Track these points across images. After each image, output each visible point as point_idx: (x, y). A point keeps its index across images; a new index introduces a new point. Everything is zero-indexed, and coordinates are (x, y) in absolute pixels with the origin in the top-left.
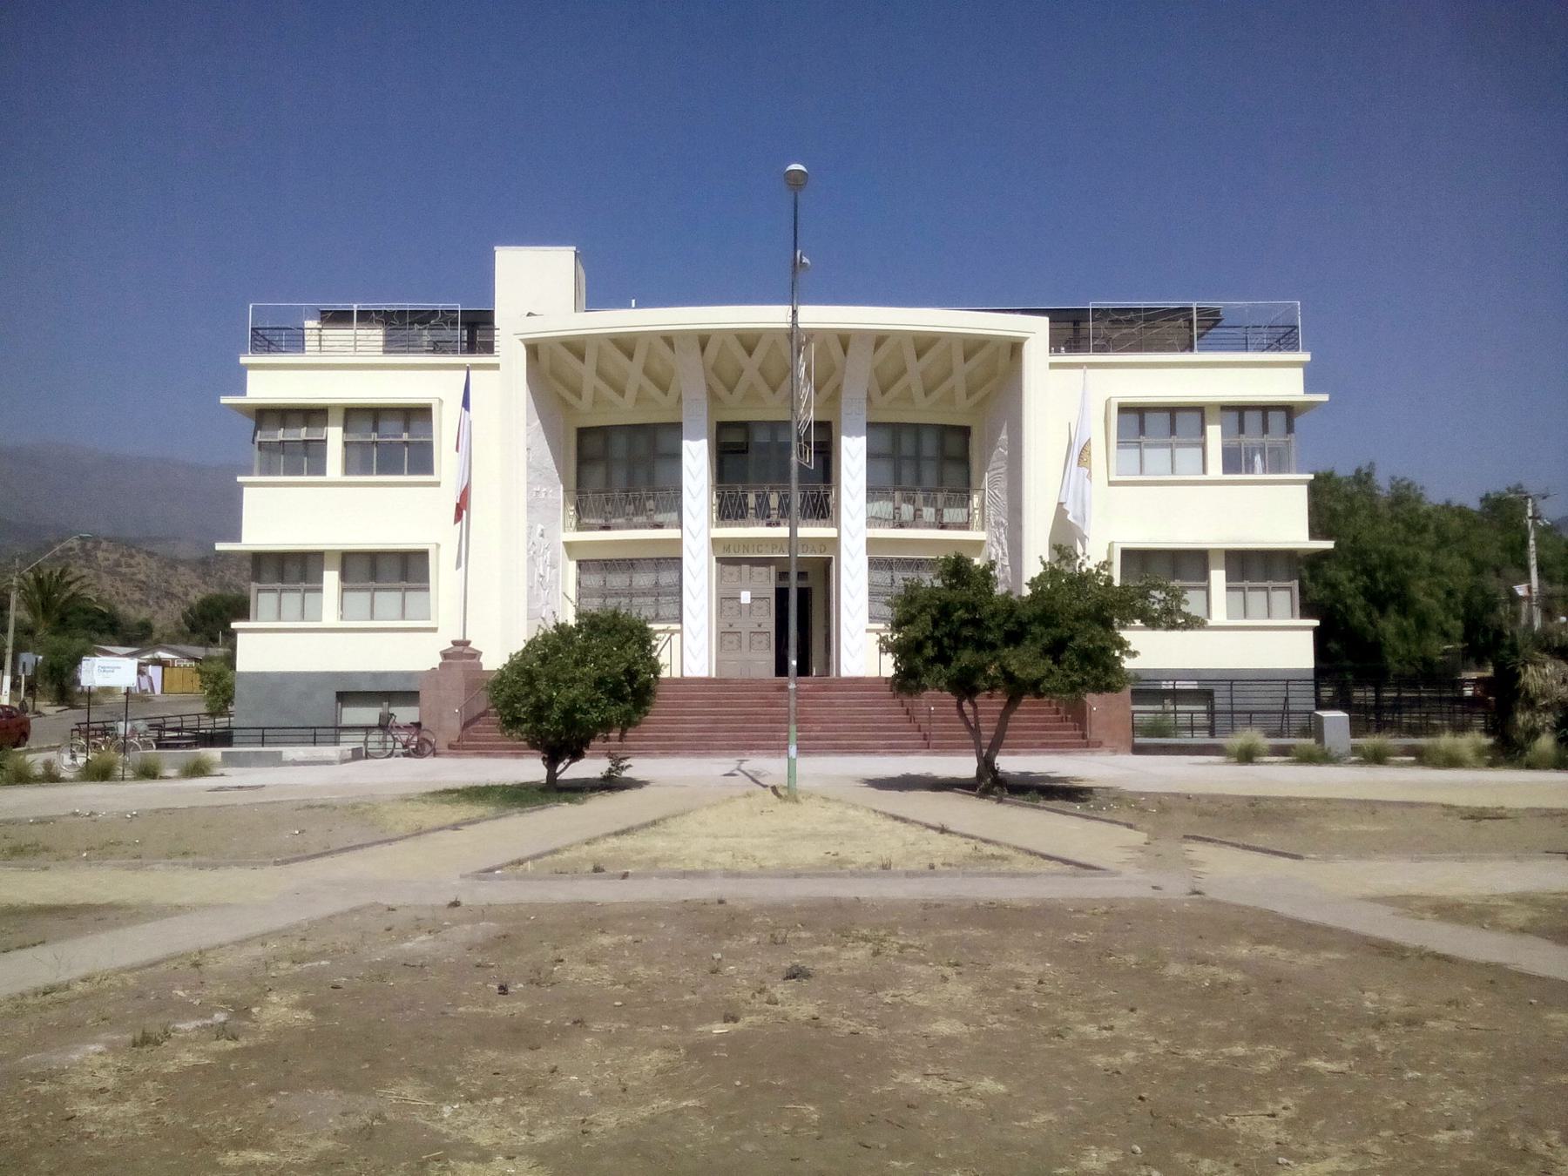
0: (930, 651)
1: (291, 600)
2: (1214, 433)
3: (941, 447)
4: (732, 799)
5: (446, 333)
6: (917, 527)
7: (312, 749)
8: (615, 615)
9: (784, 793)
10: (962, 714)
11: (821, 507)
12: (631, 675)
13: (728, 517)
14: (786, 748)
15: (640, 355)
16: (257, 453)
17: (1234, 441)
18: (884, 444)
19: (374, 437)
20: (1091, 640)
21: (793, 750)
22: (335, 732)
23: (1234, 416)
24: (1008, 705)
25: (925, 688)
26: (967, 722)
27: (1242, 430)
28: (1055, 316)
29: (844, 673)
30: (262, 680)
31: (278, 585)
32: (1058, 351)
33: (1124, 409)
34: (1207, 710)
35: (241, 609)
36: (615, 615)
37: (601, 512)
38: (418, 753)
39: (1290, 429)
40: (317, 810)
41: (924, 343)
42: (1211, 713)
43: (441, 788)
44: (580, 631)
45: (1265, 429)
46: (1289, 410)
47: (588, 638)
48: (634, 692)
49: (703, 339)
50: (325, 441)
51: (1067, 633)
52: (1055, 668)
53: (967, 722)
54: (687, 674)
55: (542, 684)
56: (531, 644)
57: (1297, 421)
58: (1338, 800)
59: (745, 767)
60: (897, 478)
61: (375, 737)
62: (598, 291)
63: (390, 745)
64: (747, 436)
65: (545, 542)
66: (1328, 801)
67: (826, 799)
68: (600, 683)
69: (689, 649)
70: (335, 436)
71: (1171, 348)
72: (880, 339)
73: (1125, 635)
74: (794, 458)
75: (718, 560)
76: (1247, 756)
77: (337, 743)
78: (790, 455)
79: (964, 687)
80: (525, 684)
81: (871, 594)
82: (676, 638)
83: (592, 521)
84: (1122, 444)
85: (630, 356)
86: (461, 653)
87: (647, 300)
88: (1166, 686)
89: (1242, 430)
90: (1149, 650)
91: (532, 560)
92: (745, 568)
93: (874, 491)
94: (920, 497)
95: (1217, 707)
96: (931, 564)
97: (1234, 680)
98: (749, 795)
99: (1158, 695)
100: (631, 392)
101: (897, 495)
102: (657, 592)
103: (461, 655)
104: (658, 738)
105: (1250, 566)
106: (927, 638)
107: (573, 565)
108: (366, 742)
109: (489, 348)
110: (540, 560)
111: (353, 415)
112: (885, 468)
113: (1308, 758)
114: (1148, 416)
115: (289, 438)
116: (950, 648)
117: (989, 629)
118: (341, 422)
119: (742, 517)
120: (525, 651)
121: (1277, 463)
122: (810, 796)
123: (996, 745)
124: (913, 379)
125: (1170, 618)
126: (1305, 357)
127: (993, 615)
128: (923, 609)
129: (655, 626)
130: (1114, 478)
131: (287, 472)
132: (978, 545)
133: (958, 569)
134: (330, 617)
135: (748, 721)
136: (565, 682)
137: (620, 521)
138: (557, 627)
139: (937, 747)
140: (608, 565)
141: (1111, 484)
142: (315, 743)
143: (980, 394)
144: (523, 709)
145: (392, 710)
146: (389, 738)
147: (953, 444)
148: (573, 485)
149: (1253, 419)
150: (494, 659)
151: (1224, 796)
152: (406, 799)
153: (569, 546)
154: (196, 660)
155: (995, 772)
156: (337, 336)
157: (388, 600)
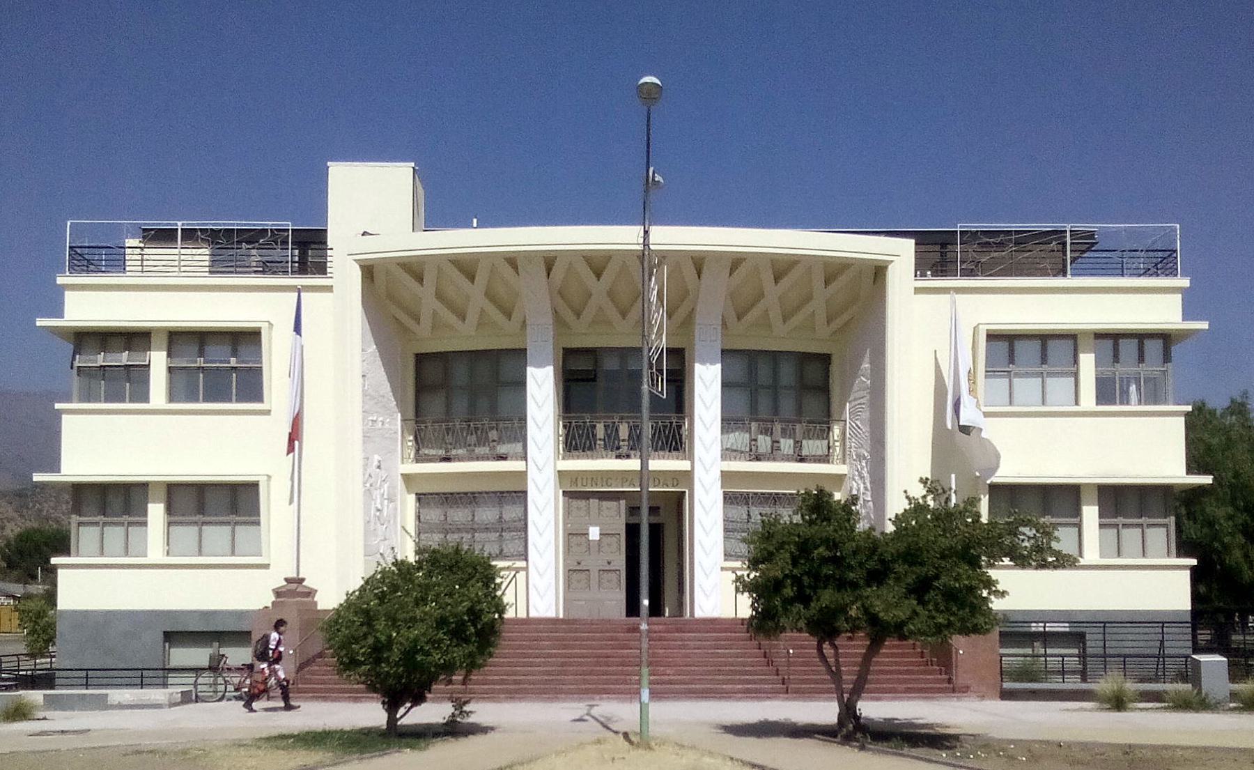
0: (788, 592)
1: (114, 534)
2: (1087, 361)
3: (801, 376)
4: (581, 745)
5: (276, 254)
6: (774, 460)
8: (457, 551)
9: (637, 739)
11: (674, 439)
12: (475, 614)
15: (607, 276)
17: (1108, 371)
18: (739, 373)
19: (200, 362)
22: (161, 674)
25: (783, 629)
27: (1116, 358)
28: (922, 239)
29: (699, 614)
31: (100, 518)
32: (923, 275)
33: (992, 337)
34: (1080, 651)
35: (62, 545)
37: (441, 443)
39: (1167, 358)
41: (782, 266)
42: (1083, 656)
43: (275, 733)
44: (420, 568)
45: (1141, 359)
46: (1166, 338)
47: (429, 575)
49: (549, 261)
50: (149, 365)
52: (919, 609)
54: (533, 614)
55: (381, 625)
59: (595, 711)
61: (206, 679)
62: (437, 210)
65: (383, 474)
66: (1205, 749)
67: (682, 746)
68: (442, 622)
69: (535, 588)
70: (158, 361)
71: (1044, 273)
72: (736, 261)
74: (645, 387)
76: (1118, 703)
77: (165, 685)
80: (362, 624)
81: (726, 530)
83: (432, 452)
84: (990, 373)
85: (471, 278)
86: (295, 590)
88: (1036, 628)
89: (1116, 358)
90: (1018, 590)
91: (368, 493)
92: (594, 502)
93: (729, 423)
94: (778, 427)
95: (1089, 651)
96: (790, 499)
97: (1106, 622)
98: (599, 742)
99: (1029, 638)
100: (472, 317)
101: (754, 425)
102: (501, 527)
103: (292, 593)
104: (502, 682)
105: (1123, 501)
106: (786, 576)
107: (411, 499)
110: (376, 494)
111: (177, 338)
112: (741, 399)
113: (1183, 704)
115: (109, 364)
116: (810, 587)
117: (851, 568)
118: (165, 345)
119: (590, 448)
121: (1154, 393)
122: (663, 742)
123: (859, 690)
125: (1041, 557)
126: (1185, 283)
128: (781, 546)
129: (499, 564)
132: (840, 479)
133: (818, 504)
134: (156, 553)
135: (598, 664)
136: (405, 621)
137: (460, 452)
138: (395, 564)
139: (797, 691)
140: (449, 499)
144: (361, 650)
150: (329, 598)
152: (240, 744)
153: (407, 478)
154: (14, 597)
156: (159, 254)
157: (217, 535)
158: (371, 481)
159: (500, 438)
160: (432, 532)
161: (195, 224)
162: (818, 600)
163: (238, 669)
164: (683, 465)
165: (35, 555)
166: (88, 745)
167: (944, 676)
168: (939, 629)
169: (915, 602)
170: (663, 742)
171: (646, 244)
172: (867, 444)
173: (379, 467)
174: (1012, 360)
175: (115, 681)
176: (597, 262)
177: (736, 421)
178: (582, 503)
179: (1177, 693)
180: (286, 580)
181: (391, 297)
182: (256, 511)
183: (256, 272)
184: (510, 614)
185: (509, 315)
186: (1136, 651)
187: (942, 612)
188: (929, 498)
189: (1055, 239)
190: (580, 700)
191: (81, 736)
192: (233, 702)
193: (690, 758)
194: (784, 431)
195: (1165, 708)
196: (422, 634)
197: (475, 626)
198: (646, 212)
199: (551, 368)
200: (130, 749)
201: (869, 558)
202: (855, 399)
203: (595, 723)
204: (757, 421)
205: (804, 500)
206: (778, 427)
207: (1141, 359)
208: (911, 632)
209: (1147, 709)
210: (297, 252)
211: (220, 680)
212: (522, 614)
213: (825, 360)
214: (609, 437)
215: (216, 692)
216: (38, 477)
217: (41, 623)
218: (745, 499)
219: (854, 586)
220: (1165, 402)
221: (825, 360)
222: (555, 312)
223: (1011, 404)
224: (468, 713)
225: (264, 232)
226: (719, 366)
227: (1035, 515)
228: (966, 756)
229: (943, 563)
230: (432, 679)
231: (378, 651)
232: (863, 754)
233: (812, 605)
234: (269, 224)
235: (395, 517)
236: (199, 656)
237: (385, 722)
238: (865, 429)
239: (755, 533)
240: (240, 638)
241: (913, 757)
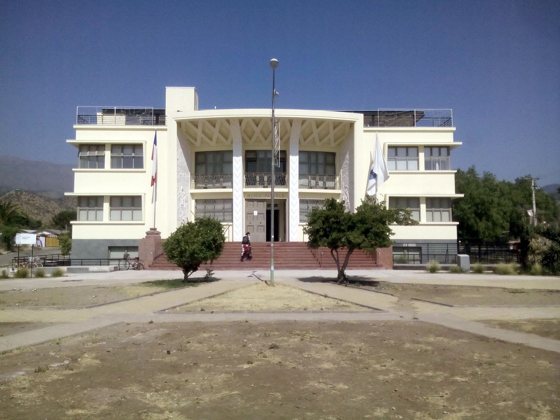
0: (321, 233)
1: (92, 213)
2: (422, 155)
5: (148, 118)
6: (317, 188)
8: (209, 219)
11: (283, 181)
12: (215, 241)
13: (249, 184)
15: (260, 125)
16: (79, 160)
17: (429, 158)
19: (122, 155)
20: (378, 229)
21: (272, 268)
22: (108, 261)
23: (394, 150)
25: (319, 246)
27: (431, 154)
28: (366, 113)
29: (291, 240)
31: (87, 208)
32: (367, 126)
33: (390, 147)
34: (419, 254)
35: (74, 216)
38: (138, 268)
39: (448, 154)
41: (319, 123)
42: (421, 255)
44: (196, 225)
45: (440, 154)
46: (448, 148)
47: (199, 227)
49: (241, 121)
50: (104, 156)
51: (370, 226)
52: (365, 239)
54: (235, 240)
55: (183, 244)
56: (179, 230)
57: (451, 152)
59: (255, 273)
61: (122, 263)
62: (202, 104)
65: (184, 193)
66: (462, 286)
67: (285, 285)
68: (203, 243)
69: (234, 232)
70: (108, 154)
72: (303, 121)
73: (391, 227)
74: (273, 164)
75: (246, 200)
76: (433, 270)
77: (108, 265)
79: (334, 245)
80: (176, 244)
81: (300, 212)
82: (231, 227)
83: (201, 185)
84: (389, 159)
85: (214, 126)
86: (153, 233)
87: (220, 107)
89: (431, 154)
90: (399, 233)
91: (179, 199)
92: (255, 203)
93: (301, 175)
94: (318, 177)
95: (423, 253)
97: (429, 243)
98: (257, 284)
101: (310, 177)
103: (153, 233)
105: (434, 203)
106: (321, 228)
107: (194, 201)
109: (163, 123)
110: (182, 200)
111: (115, 147)
112: (306, 167)
113: (455, 271)
114: (398, 149)
117: (342, 225)
119: (254, 184)
120: (176, 232)
121: (444, 166)
123: (345, 266)
124: (315, 135)
125: (406, 221)
127: (344, 220)
131: (91, 167)
132: (338, 195)
134: (106, 219)
138: (188, 223)
139: (324, 267)
140: (206, 201)
142: (100, 265)
143: (340, 140)
144: (176, 253)
145: (128, 253)
146: (127, 263)
147: (330, 159)
149: (435, 151)
152: (133, 285)
153: (192, 194)
155: (344, 276)
156: (109, 118)
157: (127, 213)
161: (121, 108)
169: (364, 237)
171: (273, 115)
176: (257, 121)
181: (187, 132)
182: (141, 206)
184: (227, 240)
185: (227, 139)
195: (449, 273)
206: (318, 177)
207: (440, 154)
208: (363, 247)
218: (307, 202)
226: (298, 156)
227: (403, 208)
234: (146, 108)
236: (120, 255)
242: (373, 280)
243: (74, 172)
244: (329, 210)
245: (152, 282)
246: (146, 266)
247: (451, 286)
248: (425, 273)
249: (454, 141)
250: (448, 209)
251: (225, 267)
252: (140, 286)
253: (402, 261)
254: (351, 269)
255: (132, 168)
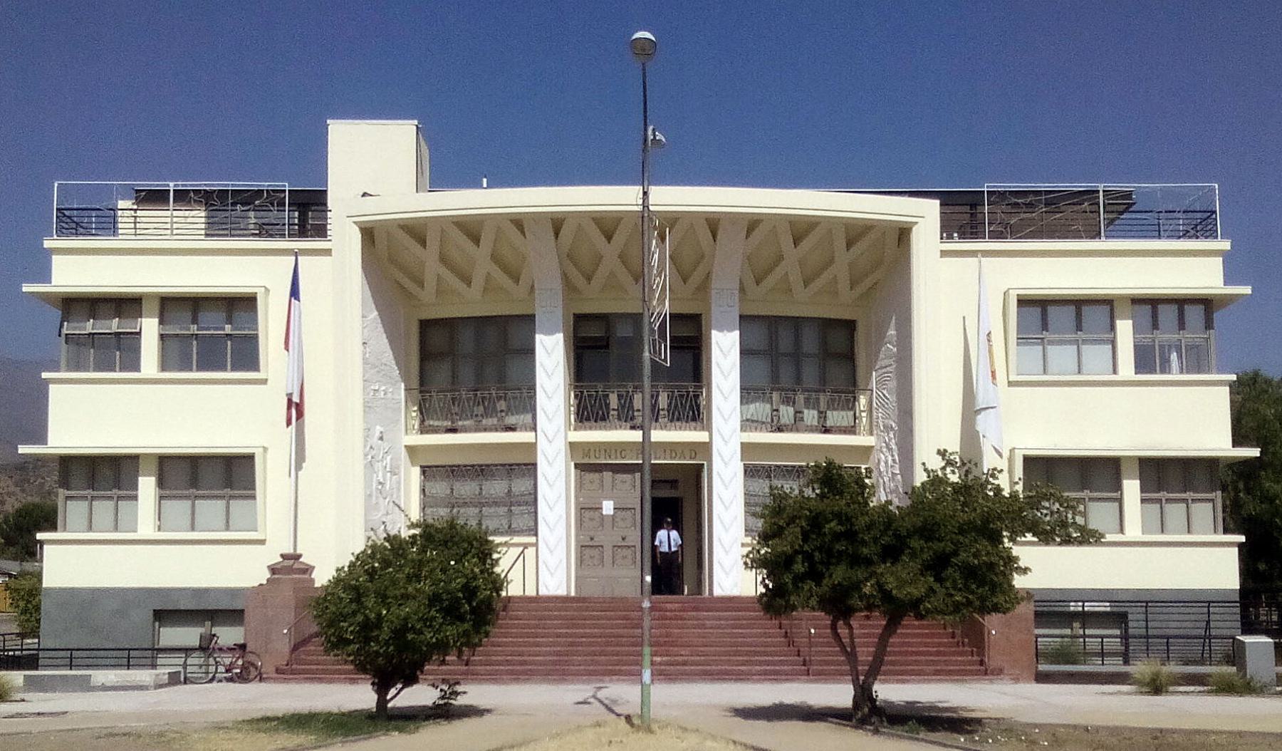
0: (799, 567)
1: (103, 509)
2: (1125, 328)
3: (824, 343)
4: (579, 728)
5: (272, 216)
6: (798, 431)
7: (124, 672)
8: (452, 525)
9: (637, 722)
10: (837, 636)
11: (692, 409)
12: (470, 591)
13: (588, 419)
14: (640, 674)
15: (619, 238)
16: (64, 346)
17: (1147, 337)
18: (760, 337)
19: (194, 329)
20: (975, 556)
21: (647, 675)
22: (150, 654)
23: (1037, 311)
24: (886, 628)
25: (794, 608)
26: (843, 646)
27: (1155, 326)
28: (947, 199)
29: (717, 592)
30: (71, 596)
31: (89, 492)
32: (950, 237)
33: (1023, 302)
34: (1123, 632)
35: (49, 520)
36: (452, 525)
37: (448, 415)
38: (243, 678)
39: (1209, 325)
40: (117, 738)
41: (801, 228)
42: (1125, 637)
43: (259, 715)
44: (413, 544)
45: (1182, 325)
46: (1208, 304)
47: (423, 550)
48: (473, 611)
49: (557, 223)
50: (139, 333)
51: (950, 548)
52: (936, 586)
53: (843, 646)
54: (543, 592)
55: (370, 602)
56: (361, 560)
57: (1216, 316)
58: (1253, 734)
59: (600, 695)
60: (775, 378)
61: (195, 660)
62: (441, 170)
63: (212, 669)
64: (608, 330)
65: (385, 445)
66: (1241, 734)
67: (685, 730)
68: (434, 599)
69: (540, 564)
70: (150, 328)
71: (1077, 235)
72: (753, 223)
73: (1016, 551)
74: (647, 354)
75: (577, 466)
76: (1156, 687)
77: (154, 666)
78: (642, 351)
79: (839, 606)
80: (351, 601)
82: (530, 552)
83: (436, 423)
84: (1022, 340)
85: (476, 240)
86: (290, 567)
88: (1074, 607)
89: (1155, 326)
90: (1042, 567)
91: (370, 466)
92: (607, 475)
93: (749, 392)
94: (800, 398)
95: (1131, 631)
96: (796, 472)
97: (1150, 601)
98: (598, 725)
99: (1067, 618)
100: (478, 281)
101: (775, 396)
102: (510, 501)
103: (290, 570)
104: (508, 663)
105: (1167, 476)
106: (796, 552)
107: (416, 471)
108: (185, 666)
110: (378, 466)
111: (170, 305)
112: (761, 368)
113: (1226, 688)
114: (1052, 310)
115: (99, 330)
116: (822, 563)
117: (864, 543)
118: (157, 312)
119: (603, 419)
120: (352, 565)
121: (1196, 361)
122: (665, 725)
123: (875, 671)
124: (790, 268)
125: (1058, 532)
126: (1226, 245)
127: (869, 527)
128: (792, 520)
129: (498, 539)
130: (1013, 378)
131: (98, 368)
132: (866, 451)
133: (835, 479)
134: (146, 527)
135: (608, 644)
136: (395, 597)
137: (467, 423)
138: (388, 539)
139: (819, 673)
140: (454, 472)
141: (1010, 384)
142: (128, 666)
143: (868, 282)
144: (349, 629)
145: (215, 630)
146: (211, 661)
147: (837, 340)
148: (415, 383)
149: (1168, 314)
150: (323, 576)
151: (1125, 728)
152: (219, 727)
153: (411, 450)
154: (10, 576)
155: (873, 700)
156: (152, 216)
157: (210, 509)
158: (373, 453)
159: (509, 409)
160: (437, 506)
161: (190, 185)
162: (831, 576)
163: (230, 649)
164: (701, 436)
165: (22, 533)
166: (58, 728)
167: (975, 658)
168: (957, 608)
169: (932, 579)
170: (665, 725)
171: (645, 205)
172: (894, 412)
173: (381, 438)
174: (1045, 326)
175: (100, 661)
176: (607, 224)
177: (756, 390)
178: (596, 476)
179: (1221, 676)
180: (282, 556)
181: (392, 260)
182: (252, 486)
183: (254, 235)
185: (517, 280)
186: (1181, 632)
187: (960, 590)
188: (948, 470)
189: (1090, 199)
190: (589, 682)
191: (56, 719)
192: (224, 684)
193: (692, 740)
194: (807, 400)
195: (1209, 692)
196: (416, 610)
197: (470, 605)
198: (644, 172)
199: (560, 337)
200: (105, 732)
201: (884, 533)
202: (882, 368)
203: (598, 704)
204: (778, 389)
205: (815, 473)
206: (800, 398)
207: (1182, 325)
208: (928, 611)
209: (1187, 693)
210: (296, 214)
211: (211, 661)
212: (531, 592)
213: (850, 326)
214: (623, 407)
215: (207, 673)
216: (23, 449)
217: (29, 598)
218: (768, 472)
219: (868, 562)
220: (1209, 372)
221: (850, 326)
222: (565, 276)
223: (1045, 372)
224: (457, 694)
225: (259, 193)
226: (737, 332)
227: (1066, 488)
228: (984, 741)
229: (961, 539)
230: (426, 659)
231: (368, 629)
232: (876, 738)
233: (825, 582)
234: (265, 185)
235: (399, 490)
236: (189, 635)
237: (374, 705)
238: (893, 398)
239: (765, 507)
240: (234, 616)
241: (926, 741)
242: (966, 715)
243: (47, 382)
244: (822, 496)
245: (278, 718)
246: (269, 669)
247: (1206, 733)
248: (1136, 693)
249: (1227, 282)
250: (1183, 495)
251: (512, 673)
252: (239, 730)
253: (1062, 656)
254: (903, 682)
255: (226, 370)
